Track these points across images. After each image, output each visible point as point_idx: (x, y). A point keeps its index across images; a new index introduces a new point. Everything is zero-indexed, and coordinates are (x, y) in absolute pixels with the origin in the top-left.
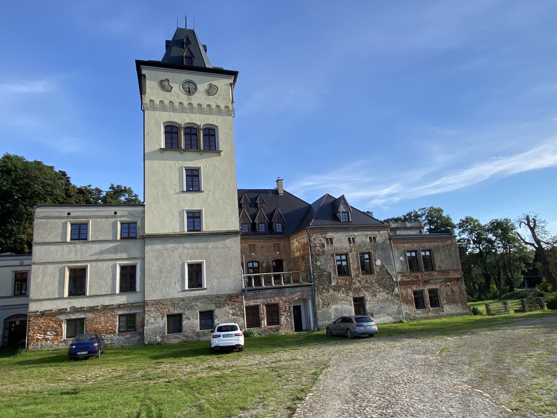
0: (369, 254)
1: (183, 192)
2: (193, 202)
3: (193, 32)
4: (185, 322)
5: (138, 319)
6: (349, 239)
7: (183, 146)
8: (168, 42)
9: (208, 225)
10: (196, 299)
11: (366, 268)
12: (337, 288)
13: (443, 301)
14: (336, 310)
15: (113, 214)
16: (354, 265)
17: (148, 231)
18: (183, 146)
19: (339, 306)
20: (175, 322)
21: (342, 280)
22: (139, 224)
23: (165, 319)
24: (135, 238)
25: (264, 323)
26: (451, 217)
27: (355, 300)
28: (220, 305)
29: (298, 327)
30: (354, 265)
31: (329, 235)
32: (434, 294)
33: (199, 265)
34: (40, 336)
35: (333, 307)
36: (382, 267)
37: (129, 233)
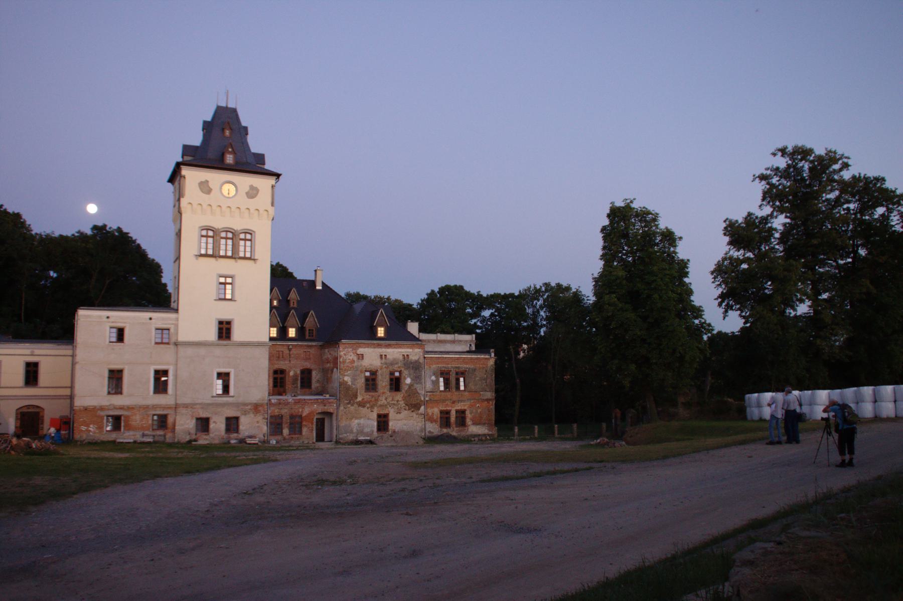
0: (400, 372)
1: (225, 299)
2: (225, 312)
3: (234, 111)
4: (212, 426)
5: (170, 420)
6: (381, 356)
7: (536, 435)
8: (205, 123)
9: (238, 334)
10: (223, 405)
11: (396, 384)
12: (362, 404)
13: (469, 421)
14: (359, 424)
15: (211, 334)
16: (383, 382)
17: (182, 338)
18: (536, 435)
19: (362, 421)
20: (204, 424)
21: (367, 396)
22: (172, 330)
23: (194, 421)
24: (168, 344)
25: (286, 431)
26: (599, 257)
27: (379, 416)
28: (245, 413)
29: (320, 437)
30: (383, 382)
31: (361, 351)
32: (461, 414)
33: (120, 371)
34: (84, 428)
35: (356, 421)
36: (410, 386)
37: (162, 338)
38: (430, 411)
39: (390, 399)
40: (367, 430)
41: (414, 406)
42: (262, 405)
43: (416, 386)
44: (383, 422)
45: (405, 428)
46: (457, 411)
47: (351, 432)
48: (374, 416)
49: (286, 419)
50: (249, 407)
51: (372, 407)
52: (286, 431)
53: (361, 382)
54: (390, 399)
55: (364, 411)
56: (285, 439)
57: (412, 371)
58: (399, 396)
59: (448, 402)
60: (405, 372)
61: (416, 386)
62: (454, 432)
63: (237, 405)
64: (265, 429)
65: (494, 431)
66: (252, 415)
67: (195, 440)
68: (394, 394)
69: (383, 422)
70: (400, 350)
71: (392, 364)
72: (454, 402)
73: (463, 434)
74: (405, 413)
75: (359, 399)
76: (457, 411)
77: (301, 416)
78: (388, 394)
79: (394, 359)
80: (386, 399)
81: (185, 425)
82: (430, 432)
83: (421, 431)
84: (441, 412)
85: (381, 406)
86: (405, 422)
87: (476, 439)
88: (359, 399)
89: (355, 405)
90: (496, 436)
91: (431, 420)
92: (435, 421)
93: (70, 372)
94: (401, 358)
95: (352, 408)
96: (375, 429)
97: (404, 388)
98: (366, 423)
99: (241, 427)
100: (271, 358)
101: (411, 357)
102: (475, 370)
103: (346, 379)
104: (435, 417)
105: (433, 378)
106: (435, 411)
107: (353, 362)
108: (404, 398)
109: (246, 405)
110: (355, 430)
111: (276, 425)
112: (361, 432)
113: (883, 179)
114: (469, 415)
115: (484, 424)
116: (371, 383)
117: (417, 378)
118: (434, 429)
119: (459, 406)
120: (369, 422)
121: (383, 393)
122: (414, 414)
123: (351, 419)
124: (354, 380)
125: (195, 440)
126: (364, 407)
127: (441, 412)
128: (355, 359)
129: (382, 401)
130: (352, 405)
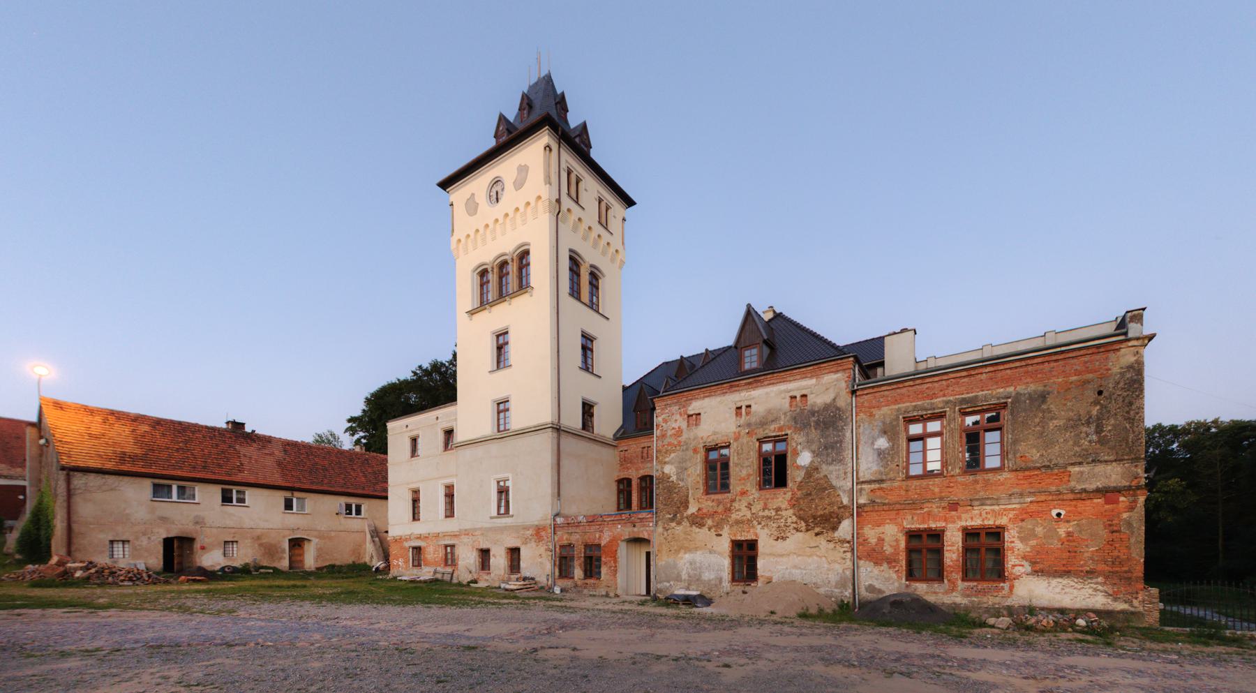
11: (775, 471)
12: (698, 521)
13: (1014, 563)
16: (744, 470)
19: (698, 556)
21: (708, 504)
27: (737, 545)
28: (525, 543)
31: (694, 407)
35: (688, 556)
36: (811, 471)
38: (871, 534)
39: (757, 507)
40: (708, 576)
41: (822, 520)
42: (544, 529)
43: (825, 469)
44: (745, 557)
45: (797, 575)
46: (969, 534)
47: (678, 578)
48: (724, 545)
49: (579, 552)
50: (530, 532)
51: (718, 527)
52: (578, 573)
53: (696, 471)
54: (757, 507)
55: (702, 534)
56: (576, 586)
57: (814, 434)
58: (781, 498)
59: (935, 508)
60: (797, 439)
61: (825, 469)
62: (950, 593)
63: (516, 528)
64: (548, 566)
65: (1146, 603)
66: (533, 544)
67: (475, 582)
68: (768, 494)
69: (745, 557)
70: (783, 387)
71: (763, 423)
72: (954, 506)
73: (990, 600)
74: (797, 539)
75: (692, 509)
76: (969, 534)
77: (599, 546)
78: (754, 493)
79: (769, 412)
80: (749, 506)
81: (467, 559)
82: (871, 588)
83: (841, 584)
84: (912, 535)
85: (737, 522)
86: (797, 560)
87: (1005, 621)
88: (692, 509)
89: (686, 523)
90: (1153, 618)
91: (876, 556)
92: (891, 561)
93: (266, 492)
94: (786, 403)
95: (680, 528)
96: (726, 574)
97: (795, 477)
98: (701, 559)
99: (522, 564)
100: (386, 460)
101: (811, 399)
102: (1043, 397)
103: (668, 469)
104: (888, 550)
105: (882, 443)
106: (891, 534)
107: (679, 432)
108: (794, 503)
109: (526, 528)
110: (684, 576)
111: (563, 564)
112: (695, 579)
113: (502, 118)
114: (1016, 547)
115: (1091, 574)
116: (718, 473)
117: (831, 449)
118: (884, 580)
119: (975, 518)
120: (713, 559)
121: (743, 493)
122: (822, 541)
123: (677, 551)
124: (682, 470)
125: (475, 582)
126: (701, 525)
127: (912, 535)
128: (684, 425)
129: (741, 511)
130: (679, 523)
